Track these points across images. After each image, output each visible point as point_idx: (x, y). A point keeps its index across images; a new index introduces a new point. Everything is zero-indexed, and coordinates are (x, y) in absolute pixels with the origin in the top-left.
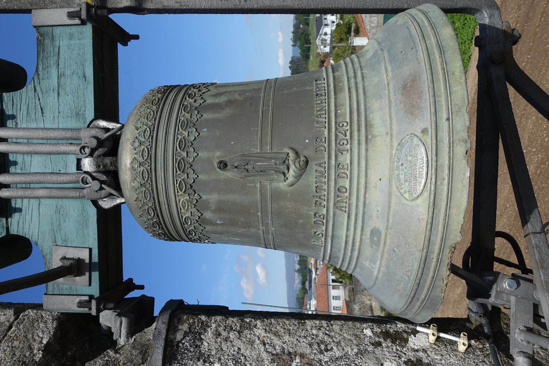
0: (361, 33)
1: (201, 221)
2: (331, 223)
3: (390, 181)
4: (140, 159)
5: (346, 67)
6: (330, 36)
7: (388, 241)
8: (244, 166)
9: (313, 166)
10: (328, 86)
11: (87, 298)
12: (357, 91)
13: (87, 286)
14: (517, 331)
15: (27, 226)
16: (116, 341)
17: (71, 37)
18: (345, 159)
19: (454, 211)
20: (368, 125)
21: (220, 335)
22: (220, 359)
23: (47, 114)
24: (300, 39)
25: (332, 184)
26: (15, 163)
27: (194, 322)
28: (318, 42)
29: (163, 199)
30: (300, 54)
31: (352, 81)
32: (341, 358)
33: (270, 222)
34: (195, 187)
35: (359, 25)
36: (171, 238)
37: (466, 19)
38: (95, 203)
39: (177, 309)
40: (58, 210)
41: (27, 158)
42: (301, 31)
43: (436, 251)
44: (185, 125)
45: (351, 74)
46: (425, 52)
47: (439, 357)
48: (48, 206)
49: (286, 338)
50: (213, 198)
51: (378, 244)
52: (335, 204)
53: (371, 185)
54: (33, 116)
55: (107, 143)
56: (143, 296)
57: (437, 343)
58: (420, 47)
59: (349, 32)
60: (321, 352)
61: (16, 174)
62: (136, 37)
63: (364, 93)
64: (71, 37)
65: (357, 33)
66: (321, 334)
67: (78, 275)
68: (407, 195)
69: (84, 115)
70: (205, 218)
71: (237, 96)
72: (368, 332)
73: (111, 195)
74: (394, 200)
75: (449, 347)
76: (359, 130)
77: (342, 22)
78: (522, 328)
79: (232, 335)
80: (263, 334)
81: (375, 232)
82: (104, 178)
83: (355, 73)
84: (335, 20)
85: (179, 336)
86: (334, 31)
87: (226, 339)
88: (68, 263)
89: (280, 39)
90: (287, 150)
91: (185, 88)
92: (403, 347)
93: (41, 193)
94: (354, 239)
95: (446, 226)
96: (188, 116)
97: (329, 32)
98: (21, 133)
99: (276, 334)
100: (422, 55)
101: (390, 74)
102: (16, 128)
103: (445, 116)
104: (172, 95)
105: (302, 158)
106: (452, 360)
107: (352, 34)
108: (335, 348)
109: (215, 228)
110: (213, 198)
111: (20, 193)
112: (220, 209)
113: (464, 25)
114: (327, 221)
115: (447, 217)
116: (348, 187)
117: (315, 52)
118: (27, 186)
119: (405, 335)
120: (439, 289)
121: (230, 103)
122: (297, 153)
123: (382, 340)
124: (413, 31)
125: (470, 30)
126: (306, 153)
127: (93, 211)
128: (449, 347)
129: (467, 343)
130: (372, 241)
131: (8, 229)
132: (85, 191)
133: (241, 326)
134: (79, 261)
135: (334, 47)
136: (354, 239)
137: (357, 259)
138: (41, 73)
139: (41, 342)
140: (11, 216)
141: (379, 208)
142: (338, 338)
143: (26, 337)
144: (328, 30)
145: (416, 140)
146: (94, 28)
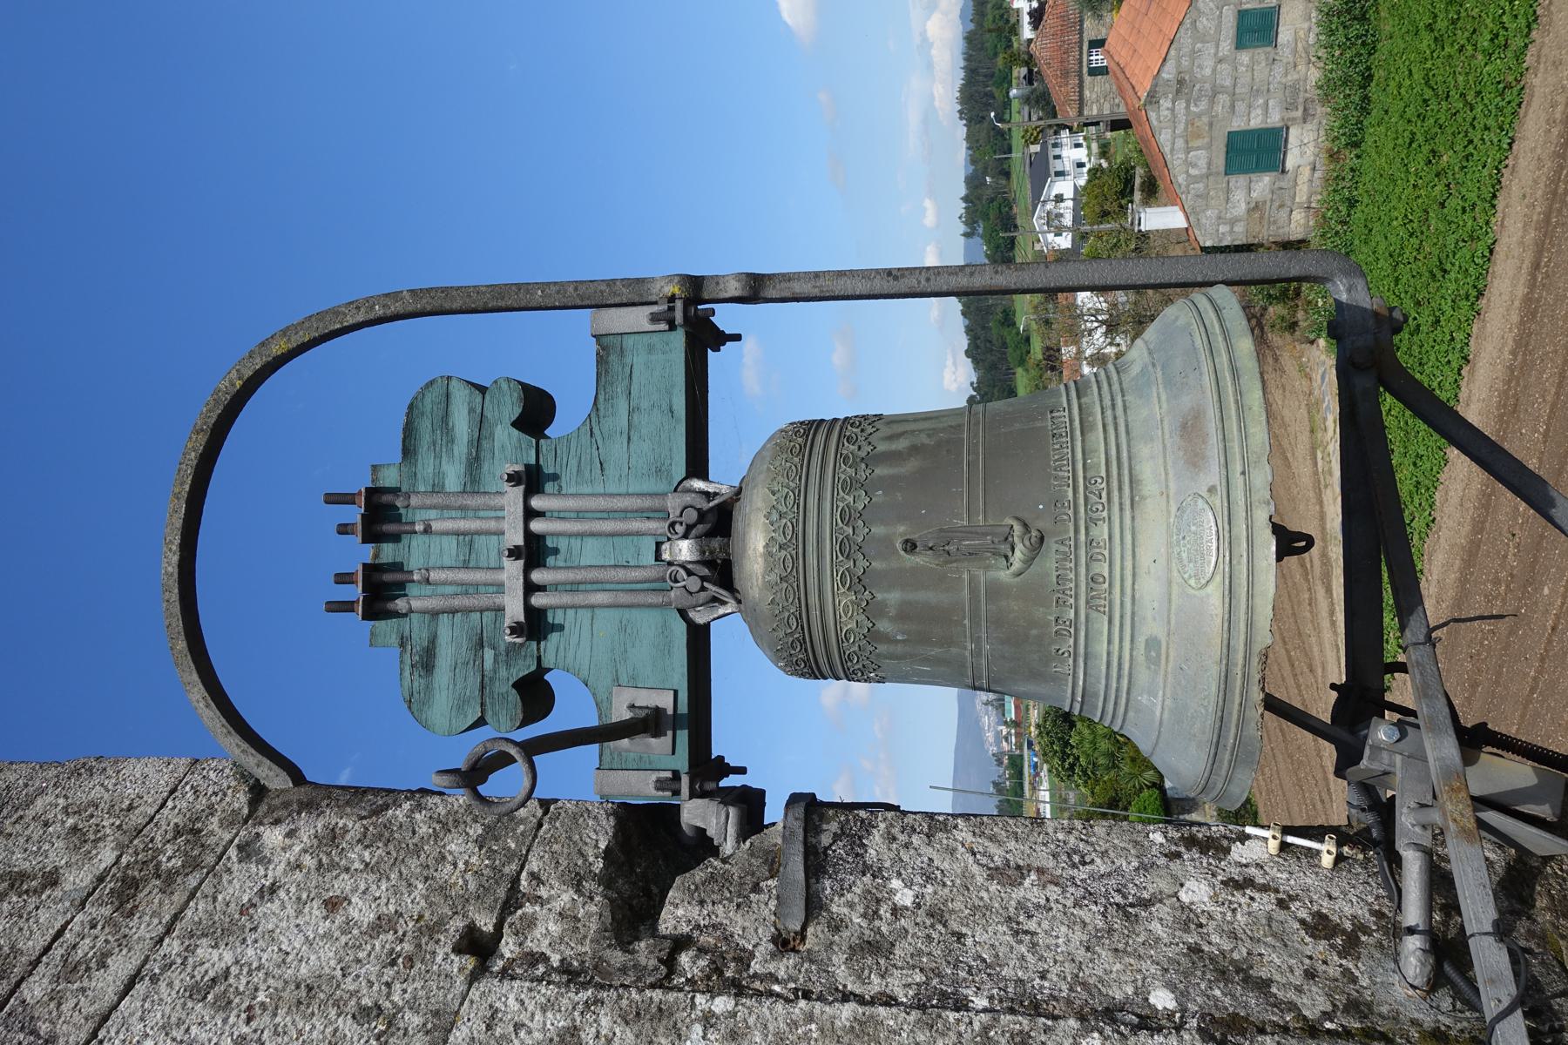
0: (1161, 194)
1: (873, 636)
2: (1082, 634)
3: (1169, 561)
4: (781, 539)
5: (1099, 388)
6: (1070, 204)
7: (1172, 654)
8: (943, 547)
9: (1051, 544)
10: (1071, 421)
11: (669, 775)
12: (1116, 429)
13: (667, 752)
14: (1405, 810)
15: (570, 654)
16: (717, 848)
17: (651, 349)
18: (1101, 532)
19: (1258, 601)
20: (1133, 481)
21: (894, 839)
22: (899, 874)
23: (610, 470)
24: (986, 217)
25: (1083, 570)
26: (556, 551)
27: (848, 820)
28: (1038, 222)
29: (814, 600)
30: (987, 256)
31: (1109, 413)
32: (1110, 874)
33: (984, 636)
34: (866, 581)
35: (1156, 174)
36: (811, 668)
37: (1471, 142)
38: (683, 613)
39: (809, 807)
40: (623, 629)
41: (576, 543)
42: (989, 193)
43: (1240, 662)
44: (850, 486)
45: (1107, 402)
46: (1213, 377)
47: (1285, 876)
48: (607, 622)
49: (1012, 845)
50: (892, 597)
51: (1157, 662)
52: (1087, 602)
53: (1141, 571)
54: (587, 474)
55: (710, 517)
56: (744, 786)
57: (1284, 855)
58: (1206, 367)
59: (1126, 191)
60: (1074, 866)
61: (555, 568)
62: (737, 338)
63: (1128, 433)
64: (651, 349)
65: (1151, 191)
66: (1072, 840)
67: (654, 736)
68: (1192, 582)
69: (669, 471)
70: (878, 632)
71: (926, 441)
72: (1158, 838)
73: (715, 600)
74: (1175, 590)
75: (1304, 861)
76: (1120, 489)
77: (1105, 165)
78: (1413, 805)
79: (915, 840)
80: (970, 838)
81: (1152, 643)
82: (705, 572)
83: (1113, 400)
84: (1085, 160)
85: (826, 840)
86: (1084, 188)
87: (907, 846)
88: (642, 714)
89: (930, 219)
90: (1011, 522)
91: (837, 428)
92: (1220, 860)
93: (600, 598)
94: (1120, 658)
95: (1250, 624)
96: (851, 471)
97: (1069, 193)
98: (571, 503)
99: (992, 838)
100: (1208, 381)
101: (1165, 405)
102: (559, 493)
103: (1239, 469)
104: (820, 438)
105: (1034, 533)
106: (1309, 881)
107: (1137, 196)
108: (1098, 861)
109: (892, 648)
110: (892, 597)
111: (566, 599)
112: (905, 614)
113: (1467, 158)
114: (1076, 630)
115: (1250, 609)
116: (1106, 575)
117: (1029, 249)
118: (573, 587)
119: (1225, 843)
120: (1253, 724)
121: (915, 450)
122: (1025, 526)
123: (1182, 849)
124: (1198, 342)
125: (1485, 172)
126: (1041, 524)
127: (680, 628)
128: (1304, 861)
129: (1334, 850)
130: (1148, 658)
131: (539, 658)
132: (672, 594)
133: (930, 827)
134: (658, 712)
135: (1084, 236)
136: (1120, 658)
137: (1128, 693)
138: (601, 407)
139: (596, 846)
140: (545, 638)
141: (1156, 605)
142: (1103, 846)
143: (570, 838)
144: (1065, 187)
145: (1200, 501)
146: (687, 333)
